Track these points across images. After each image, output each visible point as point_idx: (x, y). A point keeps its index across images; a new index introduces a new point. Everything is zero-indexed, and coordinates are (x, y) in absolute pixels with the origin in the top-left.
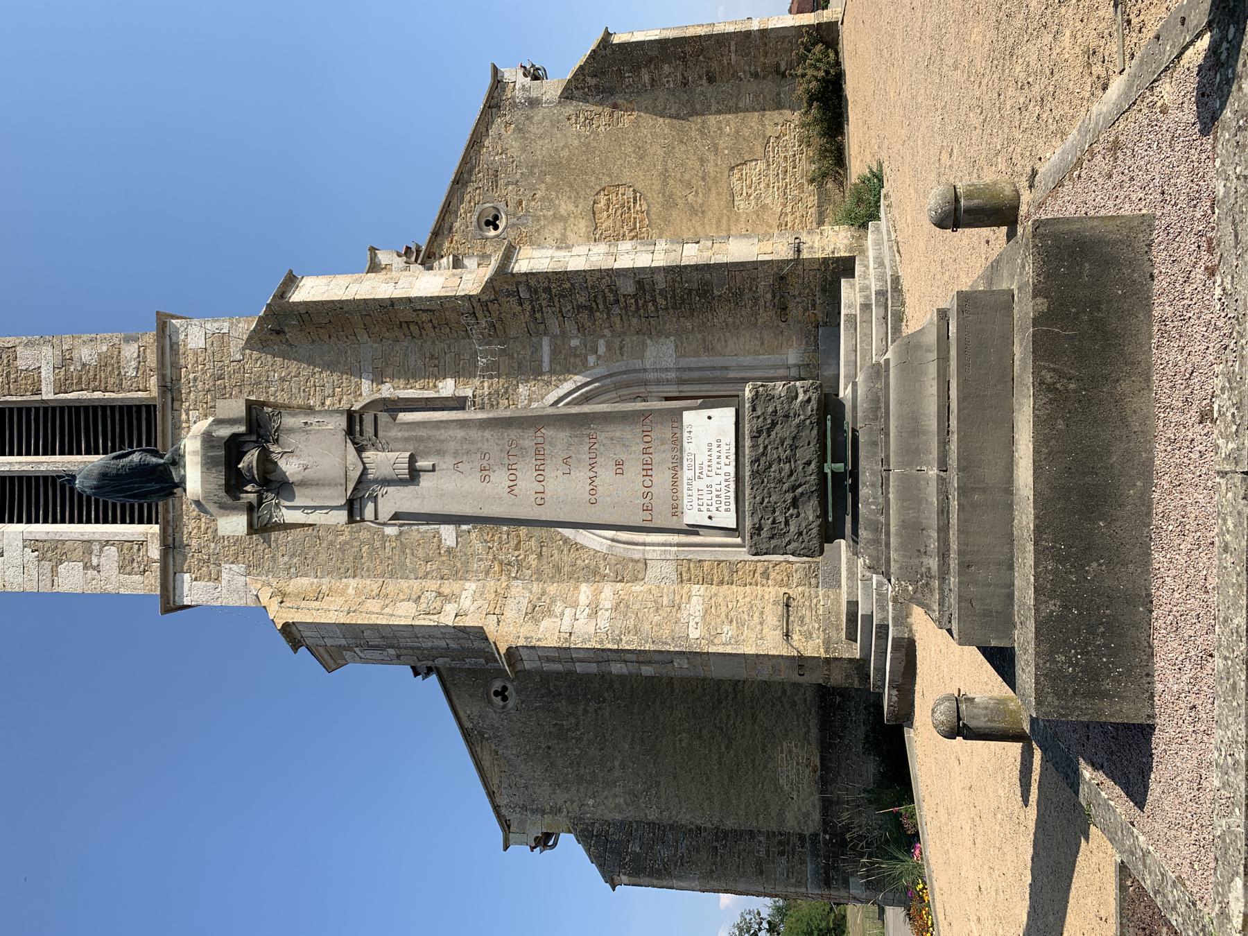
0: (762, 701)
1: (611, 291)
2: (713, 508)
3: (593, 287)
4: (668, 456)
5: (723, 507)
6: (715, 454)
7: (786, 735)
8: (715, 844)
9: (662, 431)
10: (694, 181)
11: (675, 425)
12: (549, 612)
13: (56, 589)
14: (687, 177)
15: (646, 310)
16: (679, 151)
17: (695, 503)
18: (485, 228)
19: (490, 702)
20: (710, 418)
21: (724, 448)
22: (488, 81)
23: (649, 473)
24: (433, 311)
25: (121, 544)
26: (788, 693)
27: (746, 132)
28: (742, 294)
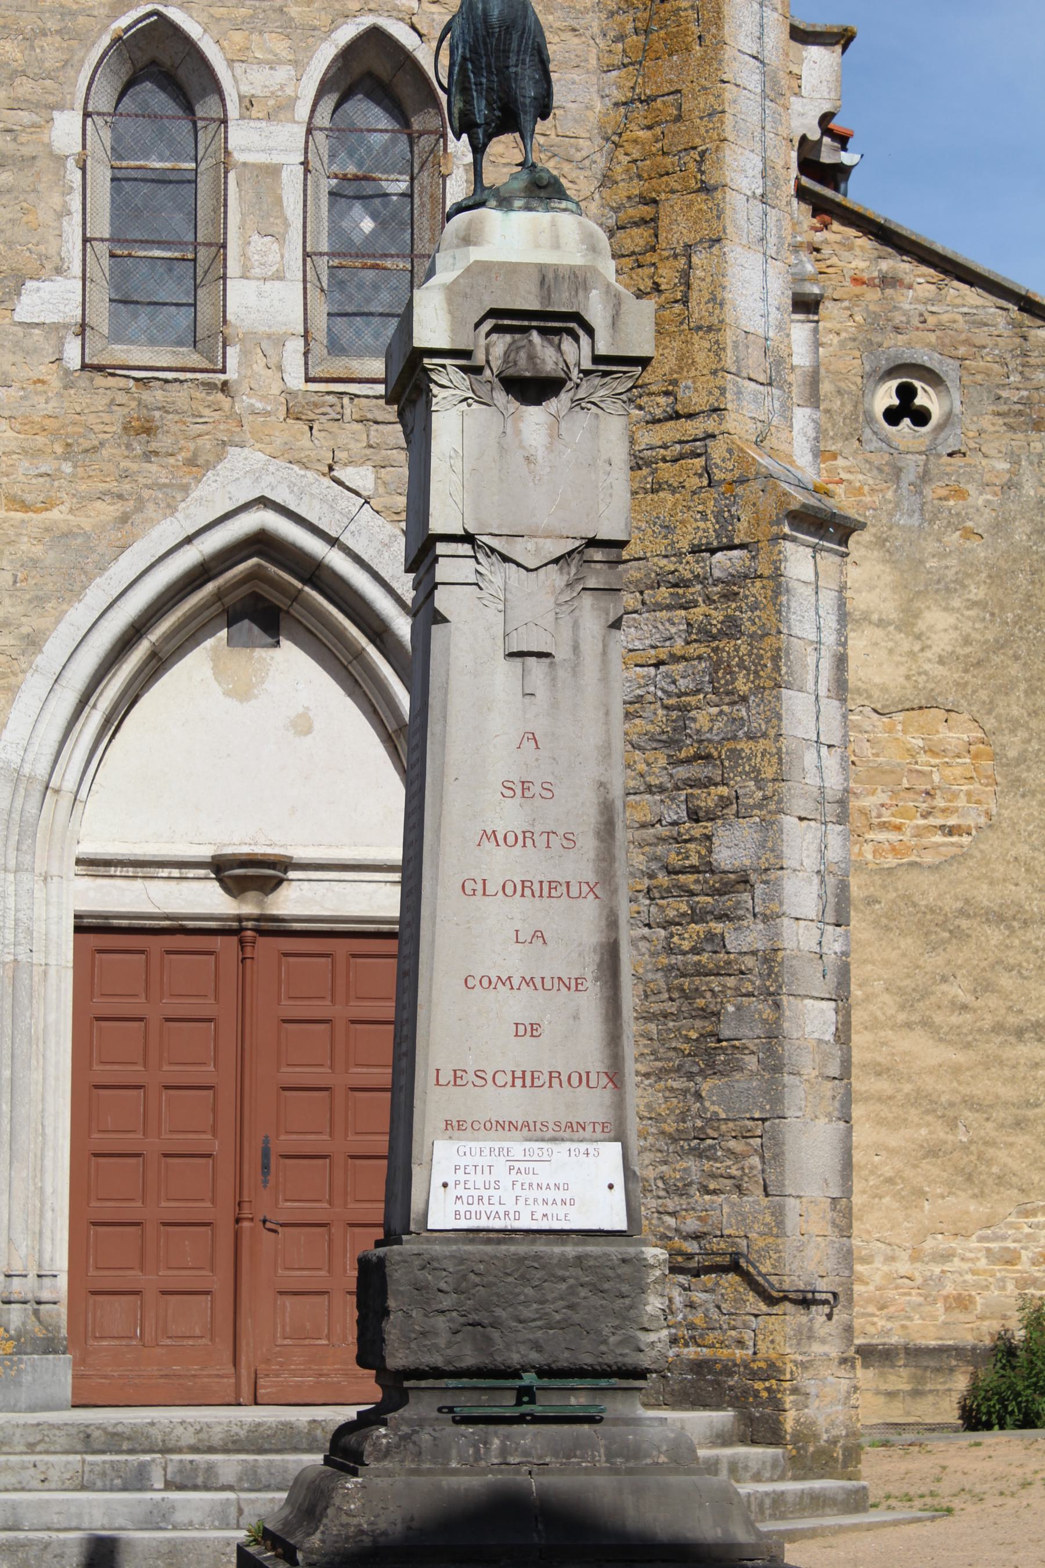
1: (724, 802)
2: (460, 1191)
6: (550, 1195)
9: (593, 1103)
10: (992, 1001)
11: (599, 1128)
14: (1006, 981)
15: (667, 893)
17: (468, 1160)
18: (894, 384)
20: (611, 1187)
21: (560, 1210)
23: (519, 1082)
24: (685, 301)
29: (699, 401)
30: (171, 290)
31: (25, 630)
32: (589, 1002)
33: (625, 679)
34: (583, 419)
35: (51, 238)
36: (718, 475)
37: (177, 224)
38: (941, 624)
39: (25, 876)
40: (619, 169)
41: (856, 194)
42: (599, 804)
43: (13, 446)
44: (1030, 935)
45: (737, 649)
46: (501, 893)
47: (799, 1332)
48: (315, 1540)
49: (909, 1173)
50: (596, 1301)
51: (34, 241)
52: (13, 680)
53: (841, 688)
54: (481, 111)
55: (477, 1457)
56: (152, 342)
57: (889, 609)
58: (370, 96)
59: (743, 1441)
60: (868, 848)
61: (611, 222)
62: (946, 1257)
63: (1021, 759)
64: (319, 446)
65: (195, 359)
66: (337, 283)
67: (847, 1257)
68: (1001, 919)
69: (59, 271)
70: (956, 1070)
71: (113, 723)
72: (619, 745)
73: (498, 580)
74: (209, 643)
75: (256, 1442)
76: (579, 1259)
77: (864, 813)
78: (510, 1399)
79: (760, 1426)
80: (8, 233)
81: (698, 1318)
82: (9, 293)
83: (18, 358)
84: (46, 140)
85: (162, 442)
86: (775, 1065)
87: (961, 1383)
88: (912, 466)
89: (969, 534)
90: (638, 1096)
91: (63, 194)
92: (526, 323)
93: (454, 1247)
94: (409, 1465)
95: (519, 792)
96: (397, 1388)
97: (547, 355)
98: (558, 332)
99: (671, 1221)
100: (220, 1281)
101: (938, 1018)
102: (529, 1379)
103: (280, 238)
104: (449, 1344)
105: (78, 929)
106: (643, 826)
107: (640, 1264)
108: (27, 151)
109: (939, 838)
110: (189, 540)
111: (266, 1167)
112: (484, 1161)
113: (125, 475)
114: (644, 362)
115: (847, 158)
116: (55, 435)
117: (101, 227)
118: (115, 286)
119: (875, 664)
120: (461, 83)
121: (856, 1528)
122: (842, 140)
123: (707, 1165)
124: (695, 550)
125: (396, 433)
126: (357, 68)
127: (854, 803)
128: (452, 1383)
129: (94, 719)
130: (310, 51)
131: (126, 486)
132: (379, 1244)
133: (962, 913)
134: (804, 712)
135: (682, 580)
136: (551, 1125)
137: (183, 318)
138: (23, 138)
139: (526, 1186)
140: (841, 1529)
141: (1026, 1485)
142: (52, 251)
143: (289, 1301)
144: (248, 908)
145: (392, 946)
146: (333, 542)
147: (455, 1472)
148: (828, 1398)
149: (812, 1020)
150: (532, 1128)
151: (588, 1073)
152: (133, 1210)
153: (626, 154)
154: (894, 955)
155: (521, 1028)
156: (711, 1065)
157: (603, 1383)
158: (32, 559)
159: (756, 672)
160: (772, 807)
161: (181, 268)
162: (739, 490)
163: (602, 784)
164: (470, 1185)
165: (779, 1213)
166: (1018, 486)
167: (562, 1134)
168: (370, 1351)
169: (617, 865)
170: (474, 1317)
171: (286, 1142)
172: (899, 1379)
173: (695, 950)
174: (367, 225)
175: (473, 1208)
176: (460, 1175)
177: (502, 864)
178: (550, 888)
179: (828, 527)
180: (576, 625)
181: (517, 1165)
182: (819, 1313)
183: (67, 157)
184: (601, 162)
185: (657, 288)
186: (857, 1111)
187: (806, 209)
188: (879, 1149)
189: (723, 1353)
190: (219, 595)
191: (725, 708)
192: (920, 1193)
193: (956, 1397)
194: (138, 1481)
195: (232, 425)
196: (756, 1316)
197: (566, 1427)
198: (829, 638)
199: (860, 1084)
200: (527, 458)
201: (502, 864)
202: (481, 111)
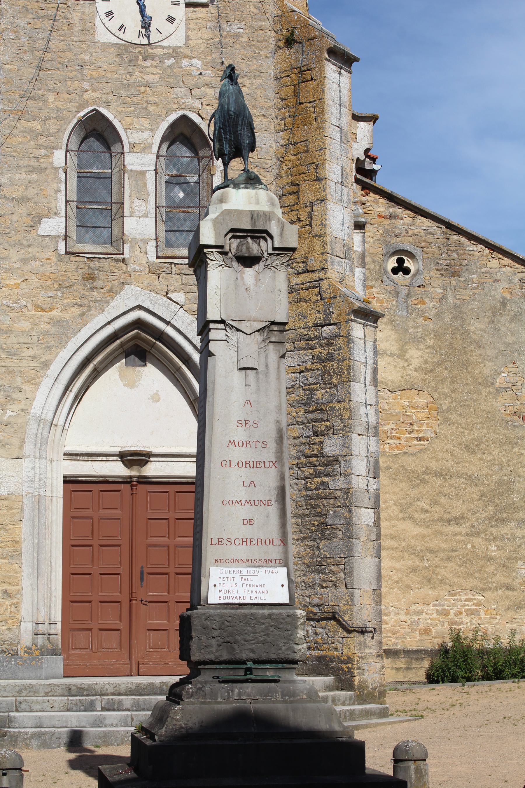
1: (328, 428)
2: (221, 588)
3: (332, 409)
4: (257, 557)
5: (222, 595)
6: (258, 589)
9: (275, 552)
10: (438, 508)
14: (443, 500)
15: (305, 465)
16: (472, 491)
17: (224, 575)
18: (396, 258)
20: (283, 586)
21: (262, 595)
23: (245, 543)
24: (310, 225)
27: (490, 568)
28: (319, 572)
29: (317, 265)
30: (102, 222)
31: (43, 360)
32: (273, 510)
33: (287, 379)
34: (269, 273)
35: (53, 201)
36: (325, 295)
37: (104, 195)
38: (415, 355)
39: (43, 460)
40: (283, 171)
41: (379, 182)
42: (277, 429)
43: (38, 285)
44: (453, 482)
45: (333, 366)
46: (237, 466)
47: (360, 644)
48: (163, 731)
49: (404, 579)
50: (277, 632)
51: (46, 202)
52: (38, 380)
53: (375, 381)
54: (227, 149)
55: (229, 697)
56: (94, 242)
57: (394, 349)
58: (182, 143)
59: (338, 689)
60: (387, 446)
61: (280, 193)
62: (420, 613)
63: (449, 410)
64: (162, 284)
65: (111, 250)
67: (380, 613)
68: (441, 475)
69: (56, 214)
70: (423, 537)
71: (79, 397)
72: (284, 405)
73: (235, 339)
74: (118, 365)
75: (139, 691)
76: (270, 615)
77: (385, 432)
79: (345, 683)
80: (35, 199)
82: (36, 223)
83: (40, 250)
84: (51, 161)
85: (98, 283)
86: (349, 535)
87: (426, 664)
88: (403, 292)
89: (426, 318)
90: (293, 548)
91: (58, 183)
92: (246, 234)
93: (219, 611)
94: (201, 700)
95: (244, 425)
96: (196, 668)
97: (254, 248)
98: (258, 238)
99: (307, 599)
100: (123, 625)
101: (416, 516)
102: (250, 664)
103: (145, 200)
104: (217, 651)
105: (65, 482)
106: (295, 438)
107: (295, 617)
108: (43, 166)
109: (415, 442)
110: (109, 323)
111: (142, 579)
112: (231, 575)
113: (83, 297)
114: (293, 250)
115: (375, 167)
116: (55, 281)
117: (73, 196)
118: (79, 220)
119: (389, 372)
120: (218, 138)
121: (384, 724)
122: (374, 160)
123: (322, 576)
124: (316, 326)
125: (193, 279)
126: (177, 132)
127: (381, 428)
128: (218, 666)
129: (71, 396)
130: (158, 125)
131: (84, 301)
132: (188, 610)
133: (425, 473)
134: (360, 391)
135: (310, 338)
136: (258, 561)
137: (106, 233)
138: (41, 161)
139: (248, 586)
140: (378, 725)
141: (453, 705)
142: (53, 206)
143: (152, 633)
144: (134, 473)
145: (192, 488)
146: (168, 323)
148: (372, 671)
149: (364, 517)
150: (250, 562)
151: (273, 539)
153: (286, 166)
155: (245, 521)
157: (280, 666)
158: (45, 331)
159: (340, 375)
160: (348, 430)
162: (333, 301)
163: (278, 421)
164: (225, 585)
165: (351, 596)
167: (262, 564)
168: (185, 654)
169: (284, 454)
170: (227, 639)
172: (401, 663)
173: (316, 489)
174: (181, 195)
175: (227, 595)
176: (221, 582)
177: (237, 454)
178: (257, 464)
179: (369, 316)
180: (267, 357)
181: (244, 577)
182: (368, 636)
183: (59, 168)
184: (276, 169)
185: (299, 220)
186: (383, 554)
187: (359, 187)
188: (392, 569)
189: (329, 653)
190: (121, 345)
191: (328, 390)
193: (424, 670)
194: (90, 707)
195: (127, 276)
196: (343, 638)
198: (370, 361)
199: (384, 543)
200: (246, 289)
201: (237, 454)
202: (227, 149)
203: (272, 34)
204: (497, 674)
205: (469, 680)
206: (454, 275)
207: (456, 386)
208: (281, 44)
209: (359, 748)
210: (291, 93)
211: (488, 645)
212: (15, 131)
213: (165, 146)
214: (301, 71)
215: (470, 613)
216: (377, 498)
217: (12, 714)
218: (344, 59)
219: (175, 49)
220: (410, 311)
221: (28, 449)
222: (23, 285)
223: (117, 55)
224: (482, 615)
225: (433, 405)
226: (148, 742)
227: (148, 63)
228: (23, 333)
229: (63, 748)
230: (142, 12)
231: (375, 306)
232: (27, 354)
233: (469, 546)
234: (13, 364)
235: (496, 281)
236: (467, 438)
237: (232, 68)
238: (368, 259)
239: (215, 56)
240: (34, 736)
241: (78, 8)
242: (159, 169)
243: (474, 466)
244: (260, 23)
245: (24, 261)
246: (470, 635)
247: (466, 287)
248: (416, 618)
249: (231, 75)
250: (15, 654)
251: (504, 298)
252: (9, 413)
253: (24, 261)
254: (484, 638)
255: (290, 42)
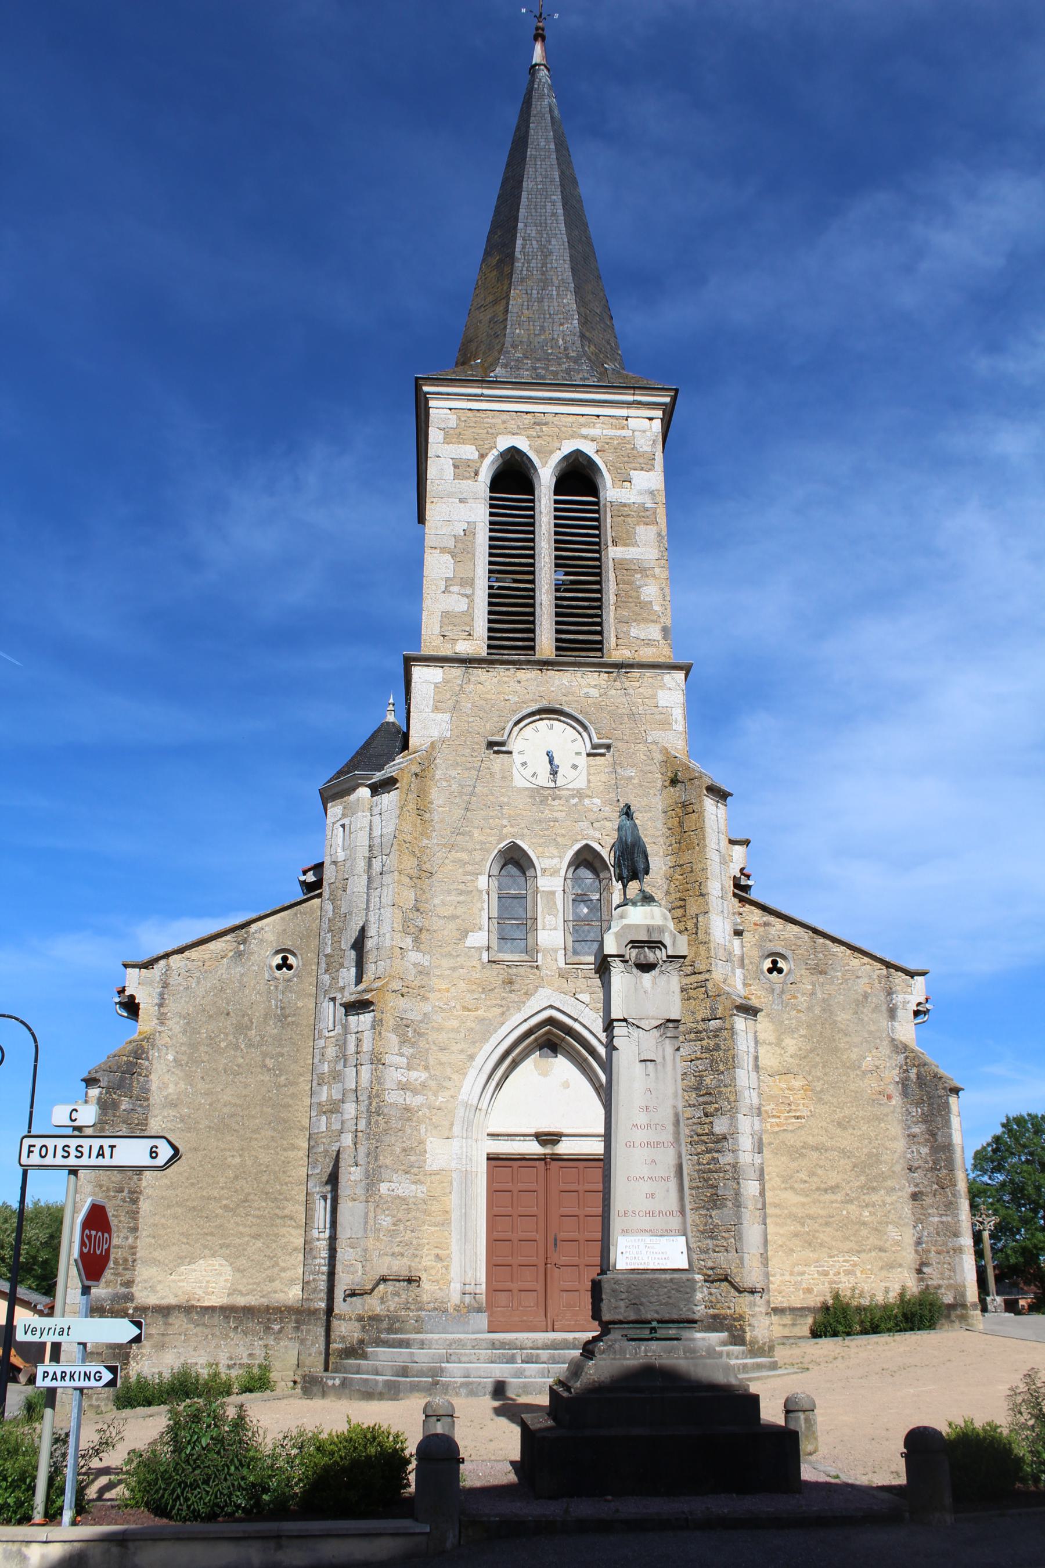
0: (274, 1246)
1: (717, 1110)
3: (720, 1092)
7: (238, 1270)
8: (126, 1191)
9: (675, 1222)
10: (815, 1179)
12: (404, 1041)
13: (427, 551)
14: (820, 1172)
15: (697, 1143)
16: (845, 1163)
19: (278, 952)
21: (664, 1262)
22: (912, 967)
24: (696, 934)
25: (469, 613)
26: (283, 1275)
27: (864, 1232)
28: (712, 1238)
29: (703, 968)
30: (518, 934)
32: (672, 1185)
33: (681, 1066)
34: (664, 977)
36: (710, 994)
37: (521, 912)
38: (791, 1043)
39: (469, 1140)
41: (753, 895)
44: (828, 1155)
47: (750, 1303)
48: (578, 1384)
49: (788, 1243)
50: (678, 1295)
53: (757, 1068)
54: (625, 873)
55: (636, 1353)
56: (512, 952)
57: (772, 1039)
58: (585, 867)
59: (731, 1344)
60: (768, 1125)
62: (803, 1274)
63: (822, 1091)
64: (570, 986)
65: (527, 958)
66: (575, 931)
67: (767, 1275)
68: (817, 1149)
69: (480, 929)
70: (803, 1205)
71: (499, 1085)
72: (680, 1091)
73: (636, 1034)
74: (533, 1056)
75: (554, 1346)
76: (671, 1280)
77: (766, 1112)
78: (648, 1332)
79: (737, 1338)
81: (713, 1299)
85: (516, 987)
86: (738, 1205)
87: (810, 1320)
88: (778, 988)
89: (799, 1011)
90: (690, 1216)
94: (612, 1356)
96: (606, 1328)
97: (651, 956)
98: (654, 947)
99: (702, 1263)
100: (540, 1286)
101: (796, 1186)
102: (654, 1324)
103: (556, 916)
105: (488, 1159)
107: (694, 1281)
108: (469, 889)
109: (794, 1120)
110: (525, 1021)
111: (556, 1244)
113: (503, 998)
114: (684, 957)
115: (749, 883)
117: (495, 914)
118: (500, 934)
119: (769, 1059)
120: (618, 865)
121: (774, 1376)
122: (748, 877)
123: (715, 1242)
124: (703, 1020)
125: (598, 982)
126: (581, 858)
127: (763, 1109)
128: (626, 1326)
129: (493, 1084)
130: (565, 853)
131: (504, 1002)
132: (598, 1275)
133: (803, 1147)
134: (744, 1077)
137: (522, 944)
140: (768, 1377)
141: (835, 1358)
143: (565, 1294)
144: (547, 1150)
145: (601, 1164)
146: (576, 1020)
147: (628, 1359)
148: (762, 1327)
149: (750, 1188)
152: (509, 1260)
154: (779, 1163)
156: (715, 1205)
157: (681, 1325)
161: (522, 927)
165: (742, 1259)
166: (815, 994)
168: (596, 1314)
170: (634, 1301)
171: (563, 1235)
172: (787, 1319)
173: (708, 1164)
174: (586, 910)
178: (657, 1144)
179: (750, 1011)
180: (664, 1050)
182: (757, 1296)
184: (666, 887)
185: (686, 929)
186: (768, 1221)
187: (737, 900)
188: (777, 1234)
189: (723, 1312)
190: (536, 1040)
192: (792, 1250)
193: (808, 1326)
194: (512, 1360)
195: (540, 980)
197: (668, 1342)
198: (752, 1050)
199: (769, 1210)
202: (625, 873)
203: (659, 776)
204: (873, 1329)
205: (848, 1334)
206: (821, 973)
207: (828, 1070)
208: (667, 784)
209: (755, 1399)
210: (676, 824)
211: (865, 1302)
212: (447, 861)
213: (572, 869)
214: (684, 805)
215: (848, 1273)
216: (762, 1170)
217: (443, 1365)
218: (720, 795)
219: (578, 790)
220: (785, 1005)
221: (456, 1130)
222: (453, 990)
223: (531, 797)
224: (859, 1274)
225: (808, 1088)
226: (565, 1394)
227: (556, 802)
228: (453, 1030)
229: (488, 1397)
230: (551, 761)
231: (754, 1002)
232: (455, 1048)
233: (845, 1212)
234: (444, 1057)
235: (858, 977)
236: (839, 1115)
237: (628, 807)
238: (746, 961)
239: (613, 795)
240: (463, 1385)
241: (498, 761)
242: (567, 890)
243: (845, 1140)
244: (649, 768)
245: (454, 969)
246: (849, 1293)
247: (832, 983)
248: (799, 1278)
249: (627, 812)
250: (446, 1311)
251: (866, 992)
252: (441, 1099)
253: (454, 969)
254: (861, 1296)
255: (674, 782)
